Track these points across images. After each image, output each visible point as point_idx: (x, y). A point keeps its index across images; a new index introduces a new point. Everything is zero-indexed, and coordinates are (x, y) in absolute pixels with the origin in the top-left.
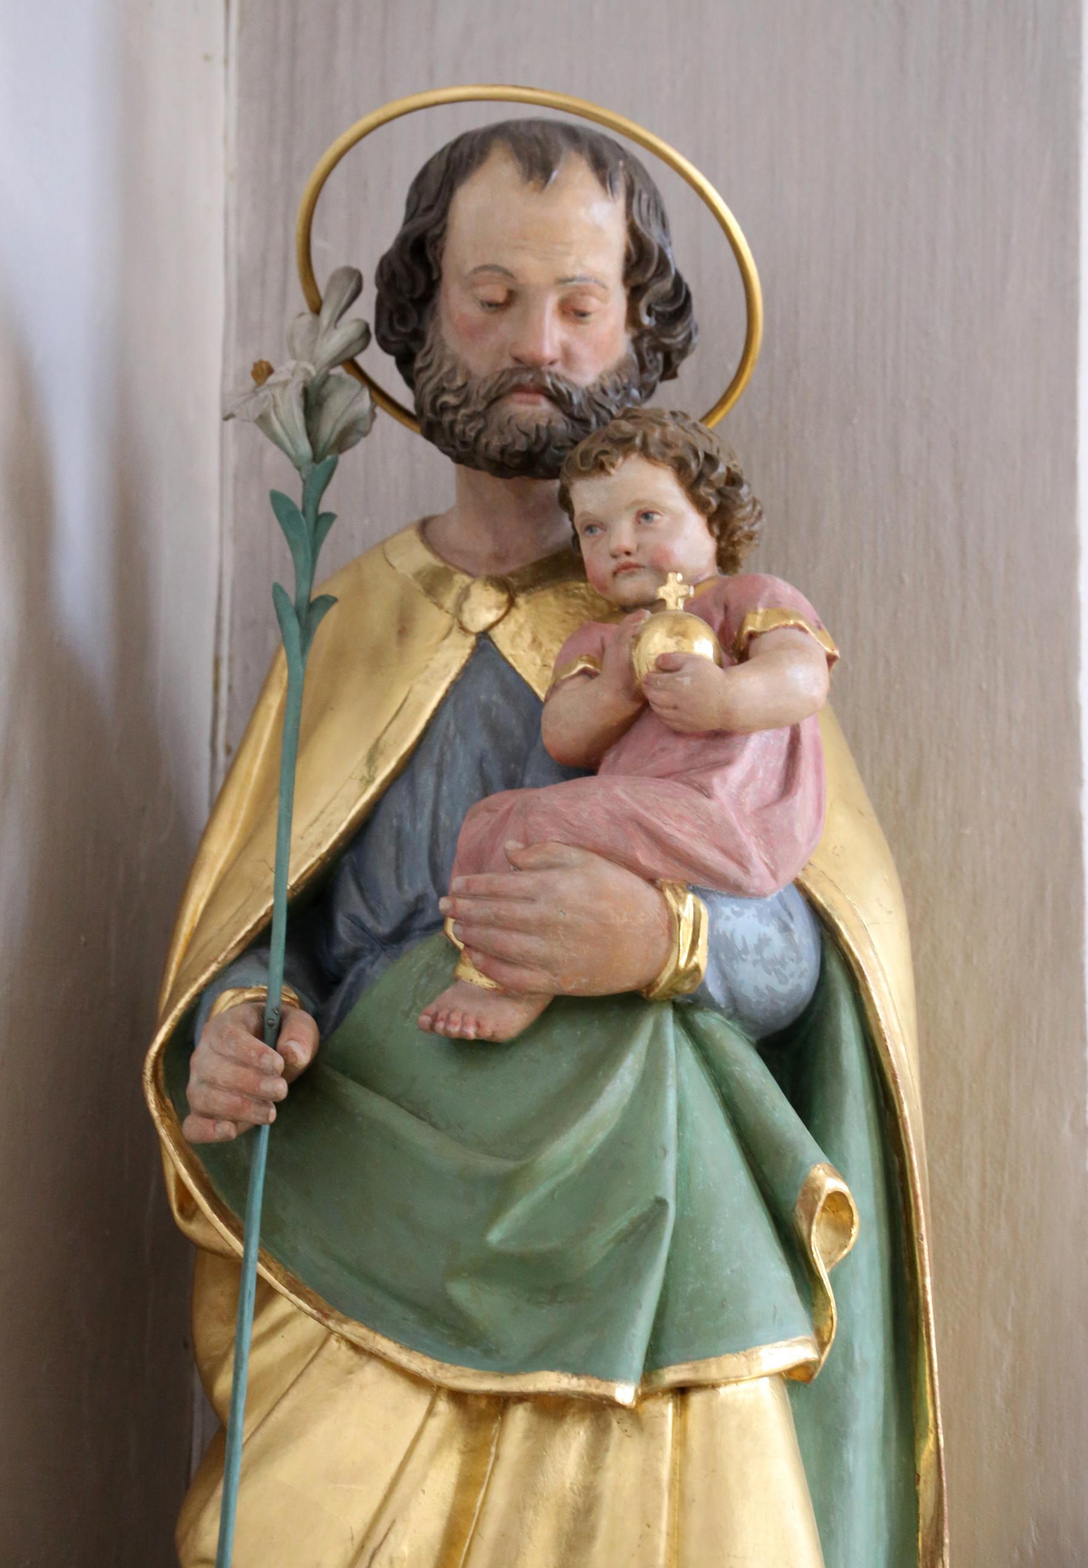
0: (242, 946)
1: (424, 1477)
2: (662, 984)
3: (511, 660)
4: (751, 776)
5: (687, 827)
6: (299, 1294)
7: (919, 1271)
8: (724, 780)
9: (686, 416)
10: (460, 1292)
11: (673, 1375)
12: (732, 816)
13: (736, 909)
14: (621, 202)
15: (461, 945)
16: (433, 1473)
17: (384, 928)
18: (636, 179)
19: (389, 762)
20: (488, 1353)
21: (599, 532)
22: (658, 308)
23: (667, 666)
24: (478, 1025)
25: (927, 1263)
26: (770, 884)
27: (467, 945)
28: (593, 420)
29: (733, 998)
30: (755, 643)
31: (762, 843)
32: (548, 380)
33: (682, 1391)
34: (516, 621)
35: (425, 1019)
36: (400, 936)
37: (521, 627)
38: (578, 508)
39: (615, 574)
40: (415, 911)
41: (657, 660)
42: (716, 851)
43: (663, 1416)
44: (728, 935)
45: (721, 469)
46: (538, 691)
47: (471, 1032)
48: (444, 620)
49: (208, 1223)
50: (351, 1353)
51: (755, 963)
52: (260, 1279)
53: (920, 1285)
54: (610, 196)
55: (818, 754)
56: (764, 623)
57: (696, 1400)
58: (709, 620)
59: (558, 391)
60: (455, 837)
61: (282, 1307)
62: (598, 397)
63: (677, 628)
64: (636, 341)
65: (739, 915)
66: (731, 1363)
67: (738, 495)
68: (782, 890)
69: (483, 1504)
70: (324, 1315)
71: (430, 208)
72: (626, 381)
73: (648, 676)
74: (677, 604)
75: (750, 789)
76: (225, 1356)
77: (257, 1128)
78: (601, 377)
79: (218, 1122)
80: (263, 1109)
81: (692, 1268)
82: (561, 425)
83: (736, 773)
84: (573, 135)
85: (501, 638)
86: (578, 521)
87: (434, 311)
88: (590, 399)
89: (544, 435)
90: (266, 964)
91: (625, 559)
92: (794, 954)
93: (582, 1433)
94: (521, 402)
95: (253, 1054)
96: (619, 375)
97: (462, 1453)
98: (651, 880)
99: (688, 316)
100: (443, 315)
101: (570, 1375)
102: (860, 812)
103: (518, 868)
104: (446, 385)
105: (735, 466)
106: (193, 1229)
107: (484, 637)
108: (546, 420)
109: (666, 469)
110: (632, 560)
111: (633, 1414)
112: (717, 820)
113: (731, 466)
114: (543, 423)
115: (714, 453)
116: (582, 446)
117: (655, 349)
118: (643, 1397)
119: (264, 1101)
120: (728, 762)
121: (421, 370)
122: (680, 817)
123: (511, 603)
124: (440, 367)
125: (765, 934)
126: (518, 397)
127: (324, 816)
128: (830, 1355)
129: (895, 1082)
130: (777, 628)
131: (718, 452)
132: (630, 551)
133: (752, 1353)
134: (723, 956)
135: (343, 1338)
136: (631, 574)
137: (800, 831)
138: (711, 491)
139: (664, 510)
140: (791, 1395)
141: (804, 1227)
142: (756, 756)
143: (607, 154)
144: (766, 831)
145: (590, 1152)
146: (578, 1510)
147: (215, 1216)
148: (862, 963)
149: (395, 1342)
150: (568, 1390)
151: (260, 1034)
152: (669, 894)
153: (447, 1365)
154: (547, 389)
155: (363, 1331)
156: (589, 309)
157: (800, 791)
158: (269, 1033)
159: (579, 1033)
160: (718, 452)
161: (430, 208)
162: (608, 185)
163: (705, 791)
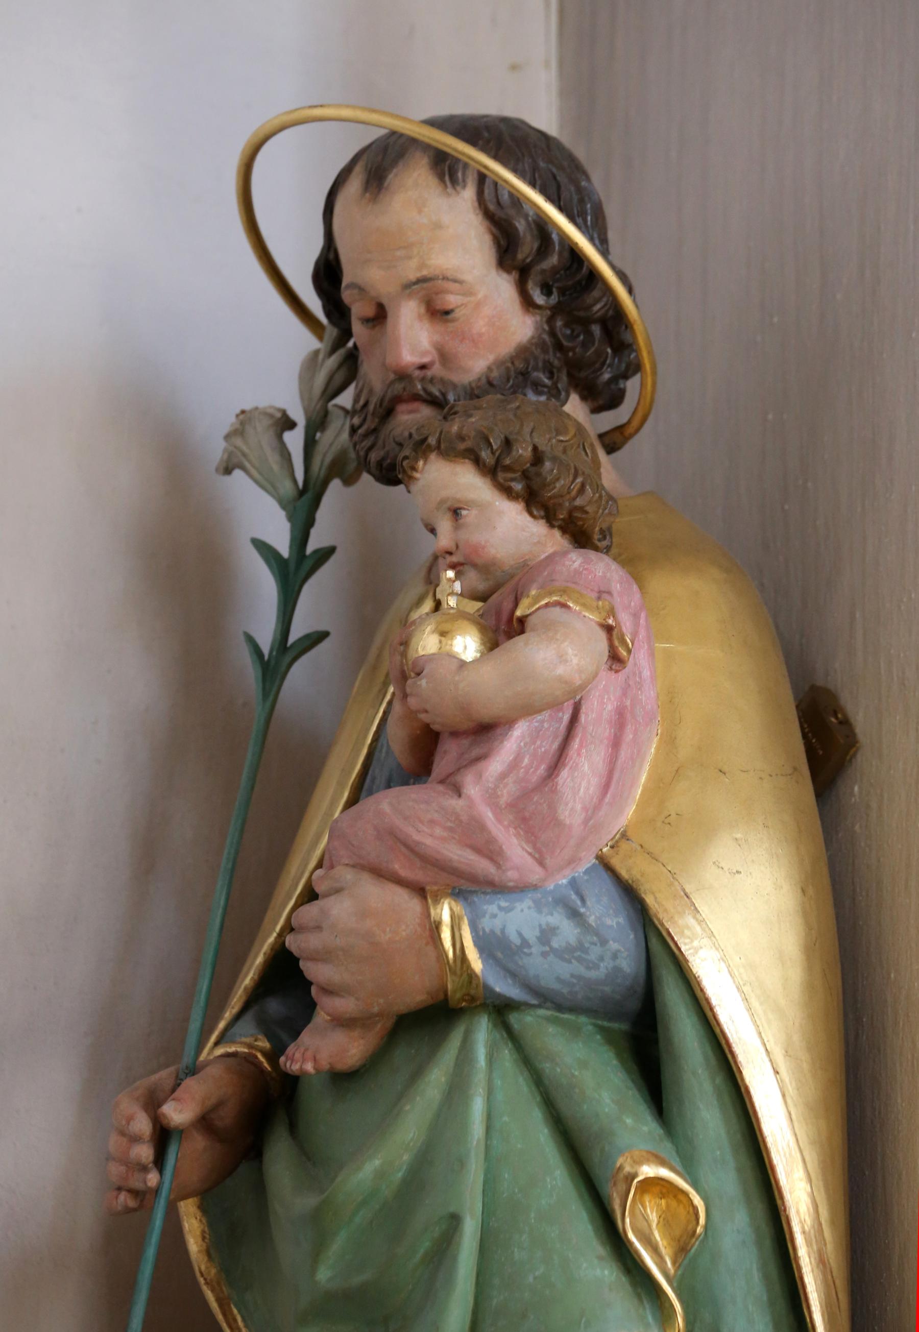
4: (514, 765)
5: (438, 831)
8: (479, 776)
13: (503, 904)
24: (315, 1060)
31: (522, 833)
42: (468, 850)
44: (498, 932)
51: (544, 955)
54: (450, 190)
75: (510, 780)
78: (490, 369)
81: (496, 1281)
83: (495, 766)
109: (465, 463)
112: (464, 818)
122: (432, 822)
132: (450, 550)
134: (499, 955)
139: (470, 504)
142: (522, 744)
145: (400, 1175)
156: (451, 307)
159: (413, 1051)
162: (447, 178)
163: (458, 791)
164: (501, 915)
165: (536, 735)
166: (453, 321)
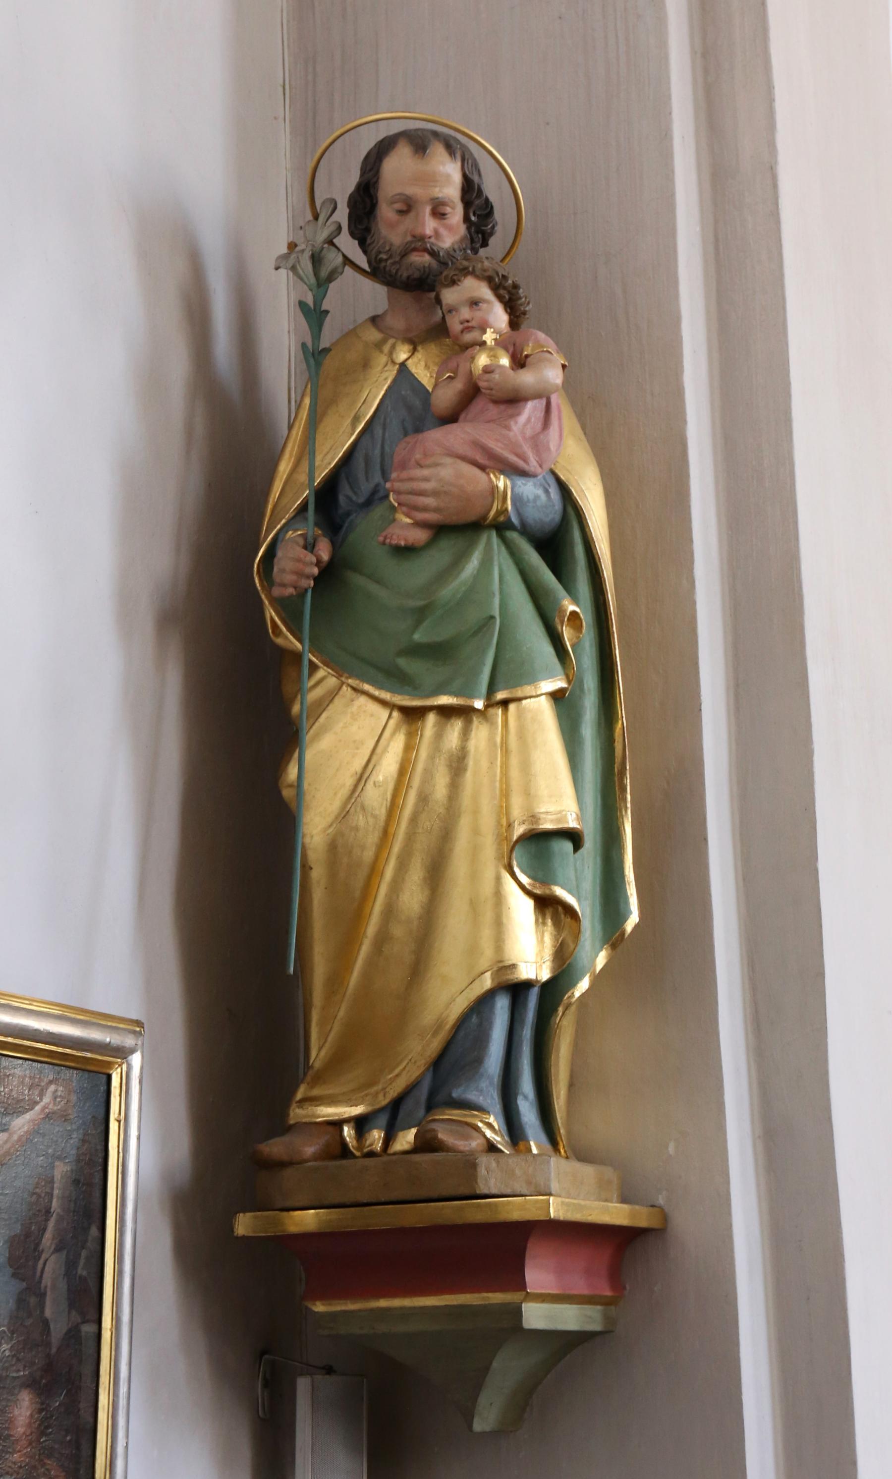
0: (296, 511)
1: (388, 745)
2: (490, 518)
3: (416, 375)
4: (529, 420)
6: (328, 666)
7: (601, 571)
8: (516, 423)
9: (492, 259)
10: (402, 662)
11: (500, 696)
12: (520, 438)
13: (524, 482)
14: (459, 164)
15: (396, 505)
16: (392, 743)
17: (361, 500)
18: (466, 153)
19: (361, 424)
20: (415, 688)
21: (454, 313)
22: (478, 213)
23: (487, 370)
25: (616, 643)
26: (539, 470)
27: (399, 504)
28: (450, 263)
29: (523, 523)
30: (529, 359)
32: (428, 245)
33: (505, 703)
34: (417, 357)
35: (381, 539)
36: (369, 503)
37: (420, 360)
38: (444, 302)
39: (462, 332)
40: (375, 491)
41: (483, 368)
43: (497, 714)
44: (520, 494)
45: (510, 282)
46: (428, 388)
47: (403, 543)
48: (383, 359)
49: (286, 638)
50: (353, 692)
52: (310, 662)
53: (614, 653)
55: (560, 411)
56: (532, 350)
57: (512, 707)
58: (506, 349)
59: (433, 250)
60: (392, 457)
61: (321, 673)
62: (452, 253)
63: (491, 353)
64: (468, 229)
65: (525, 485)
66: (528, 690)
67: (518, 293)
68: (545, 474)
69: (415, 757)
70: (339, 676)
71: (370, 170)
72: (464, 246)
73: (479, 375)
74: (491, 342)
75: (529, 426)
76: (296, 697)
77: (306, 590)
78: (453, 244)
79: (287, 588)
80: (308, 581)
82: (434, 263)
83: (522, 419)
84: (435, 134)
85: (409, 363)
86: (444, 308)
87: (375, 217)
88: (448, 252)
89: (427, 270)
90: (306, 519)
91: (466, 324)
93: (460, 723)
94: (416, 256)
95: (302, 556)
96: (461, 244)
97: (406, 735)
98: (483, 468)
99: (493, 216)
100: (379, 219)
101: (453, 697)
103: (421, 467)
104: (382, 250)
105: (516, 281)
106: (279, 641)
107: (403, 365)
108: (428, 263)
110: (470, 324)
111: (482, 713)
113: (514, 281)
114: (427, 265)
115: (506, 274)
116: (445, 273)
117: (477, 232)
118: (487, 706)
119: (308, 577)
120: (519, 414)
121: (370, 244)
123: (414, 350)
124: (378, 242)
125: (537, 494)
126: (415, 253)
127: (332, 450)
128: (573, 686)
129: (600, 562)
130: (537, 352)
131: (508, 274)
133: (537, 685)
134: (518, 504)
135: (349, 685)
136: (470, 331)
137: (553, 446)
138: (505, 292)
140: (555, 703)
141: (559, 628)
143: (452, 142)
144: (537, 446)
146: (459, 758)
147: (288, 633)
148: (582, 507)
149: (373, 686)
150: (452, 704)
151: (305, 547)
152: (492, 476)
153: (396, 695)
154: (428, 249)
155: (357, 682)
156: (447, 212)
157: (552, 428)
158: (309, 547)
160: (508, 274)
161: (370, 170)
162: (453, 157)
163: (508, 428)
164: (522, 486)
165: (535, 409)
166: (444, 219)
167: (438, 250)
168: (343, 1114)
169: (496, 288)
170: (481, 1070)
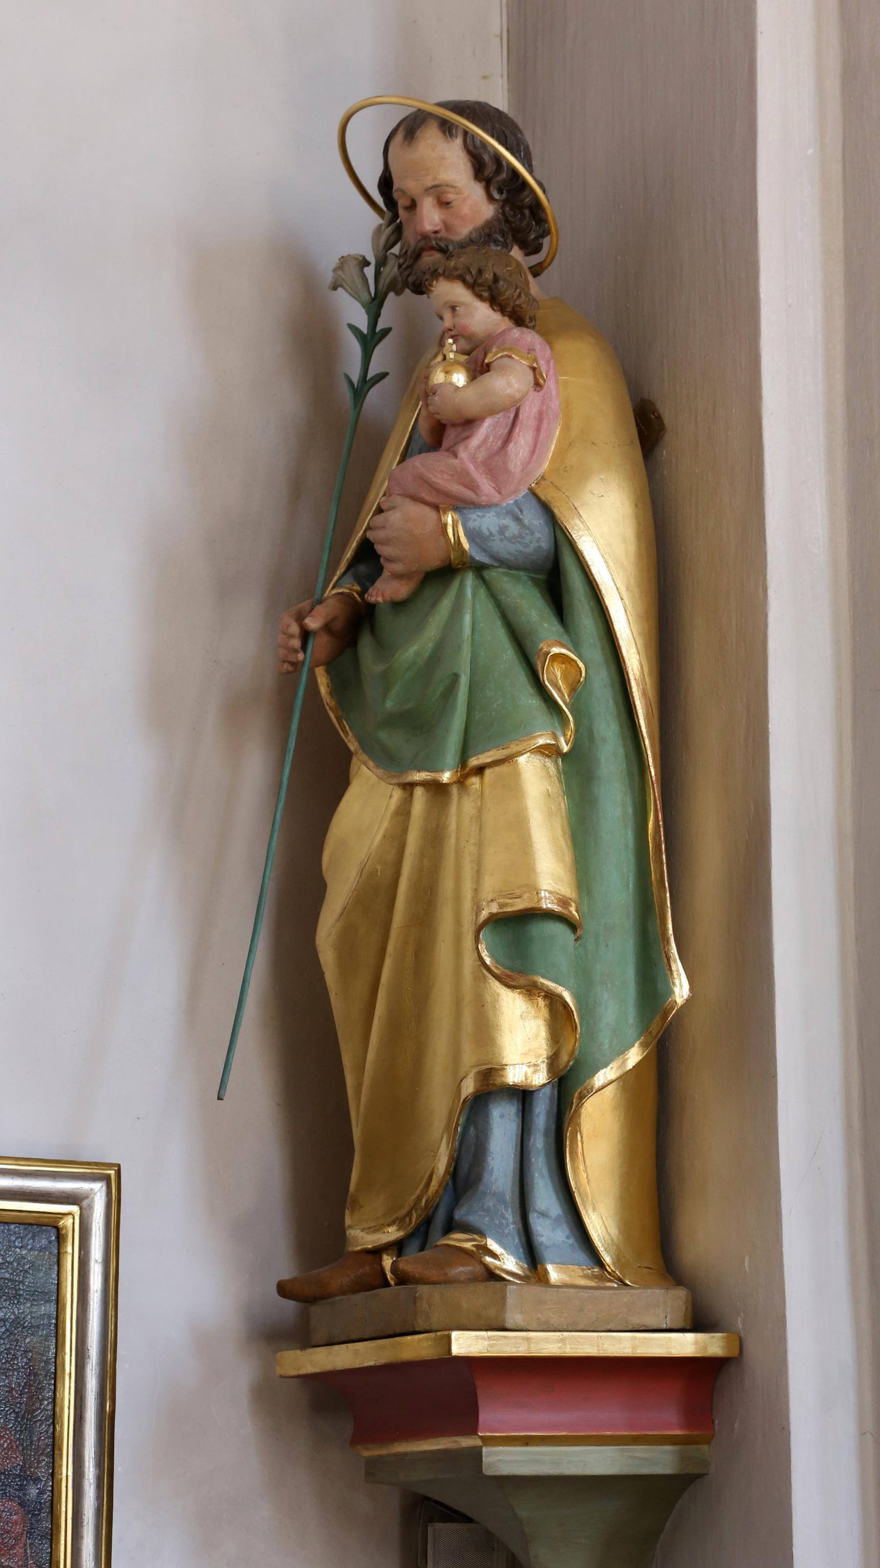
4: (485, 441)
8: (467, 447)
11: (474, 762)
13: (480, 514)
24: (383, 596)
44: (477, 529)
51: (501, 540)
59: (439, 246)
75: (483, 449)
83: (475, 442)
92: (528, 531)
102: (606, 443)
125: (503, 524)
134: (478, 540)
139: (461, 304)
156: (449, 200)
162: (447, 133)
164: (479, 519)
165: (496, 425)
166: (450, 208)
167: (445, 245)
168: (377, 1241)
169: (473, 287)
170: (481, 1188)
